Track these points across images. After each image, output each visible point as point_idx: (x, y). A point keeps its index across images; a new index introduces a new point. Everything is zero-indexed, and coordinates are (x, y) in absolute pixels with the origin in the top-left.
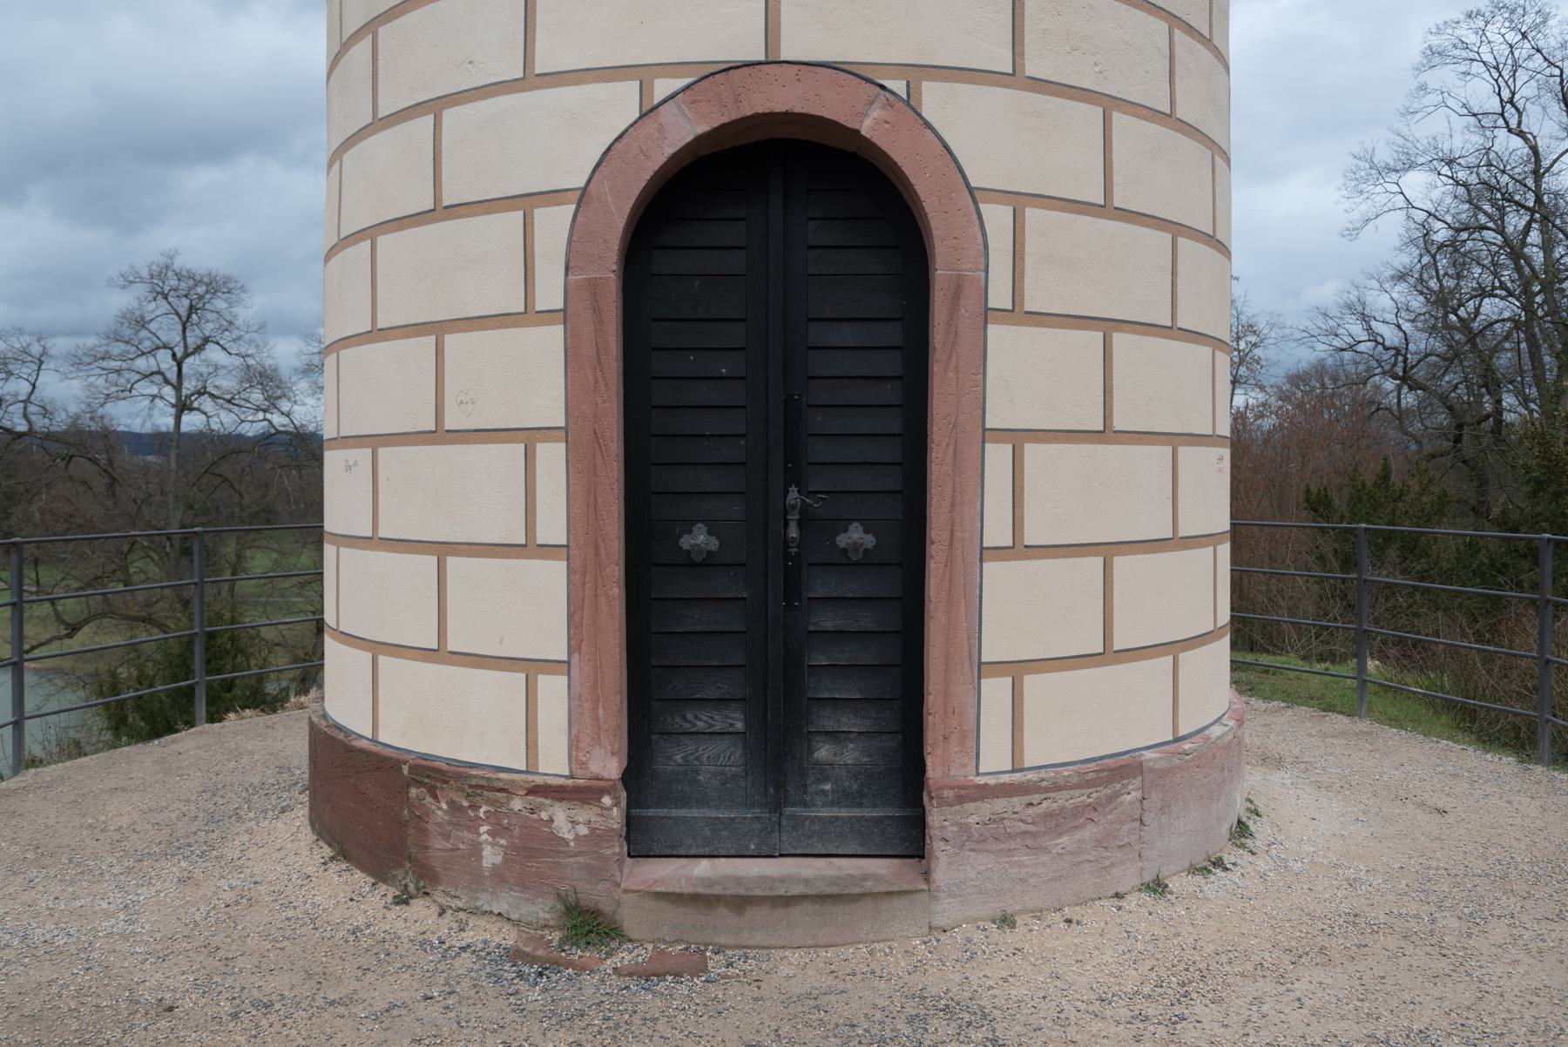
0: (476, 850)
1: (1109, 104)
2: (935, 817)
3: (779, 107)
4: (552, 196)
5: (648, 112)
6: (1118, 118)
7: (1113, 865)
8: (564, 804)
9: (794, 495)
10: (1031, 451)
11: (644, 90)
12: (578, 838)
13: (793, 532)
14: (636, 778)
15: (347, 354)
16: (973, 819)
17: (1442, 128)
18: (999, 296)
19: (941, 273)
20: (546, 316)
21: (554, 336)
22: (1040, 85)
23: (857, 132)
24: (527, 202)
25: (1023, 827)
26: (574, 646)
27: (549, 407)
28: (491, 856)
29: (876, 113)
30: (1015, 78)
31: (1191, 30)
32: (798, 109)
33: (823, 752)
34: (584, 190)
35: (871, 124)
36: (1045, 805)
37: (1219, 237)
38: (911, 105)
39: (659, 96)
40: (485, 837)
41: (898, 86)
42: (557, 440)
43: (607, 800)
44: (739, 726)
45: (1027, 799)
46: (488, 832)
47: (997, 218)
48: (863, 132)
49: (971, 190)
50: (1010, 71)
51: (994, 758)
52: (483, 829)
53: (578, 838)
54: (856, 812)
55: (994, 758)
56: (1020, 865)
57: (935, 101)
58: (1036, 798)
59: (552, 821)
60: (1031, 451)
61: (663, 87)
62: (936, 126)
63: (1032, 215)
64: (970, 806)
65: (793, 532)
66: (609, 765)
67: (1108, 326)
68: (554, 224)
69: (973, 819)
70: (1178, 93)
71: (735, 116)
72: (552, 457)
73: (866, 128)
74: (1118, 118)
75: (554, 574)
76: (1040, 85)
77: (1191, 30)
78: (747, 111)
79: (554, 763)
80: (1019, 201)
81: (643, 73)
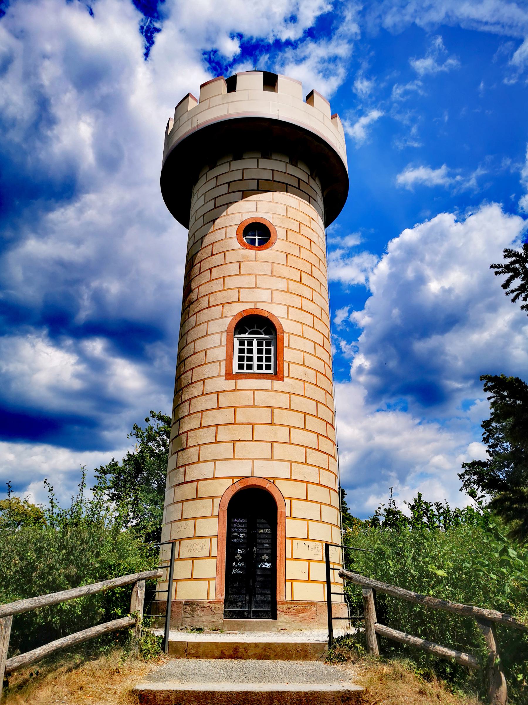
1: (307, 483)
7: (311, 622)
10: (295, 584)
11: (233, 480)
15: (176, 523)
23: (265, 488)
24: (213, 497)
25: (293, 611)
29: (268, 485)
31: (331, 456)
35: (268, 486)
41: (272, 481)
43: (222, 603)
45: (294, 605)
47: (288, 502)
49: (283, 497)
56: (293, 618)
60: (295, 584)
61: (236, 480)
63: (293, 501)
64: (284, 606)
67: (308, 520)
68: (217, 501)
70: (321, 480)
73: (267, 487)
75: (225, 348)
76: (294, 480)
77: (331, 456)
79: (212, 598)
80: (291, 499)
81: (232, 478)
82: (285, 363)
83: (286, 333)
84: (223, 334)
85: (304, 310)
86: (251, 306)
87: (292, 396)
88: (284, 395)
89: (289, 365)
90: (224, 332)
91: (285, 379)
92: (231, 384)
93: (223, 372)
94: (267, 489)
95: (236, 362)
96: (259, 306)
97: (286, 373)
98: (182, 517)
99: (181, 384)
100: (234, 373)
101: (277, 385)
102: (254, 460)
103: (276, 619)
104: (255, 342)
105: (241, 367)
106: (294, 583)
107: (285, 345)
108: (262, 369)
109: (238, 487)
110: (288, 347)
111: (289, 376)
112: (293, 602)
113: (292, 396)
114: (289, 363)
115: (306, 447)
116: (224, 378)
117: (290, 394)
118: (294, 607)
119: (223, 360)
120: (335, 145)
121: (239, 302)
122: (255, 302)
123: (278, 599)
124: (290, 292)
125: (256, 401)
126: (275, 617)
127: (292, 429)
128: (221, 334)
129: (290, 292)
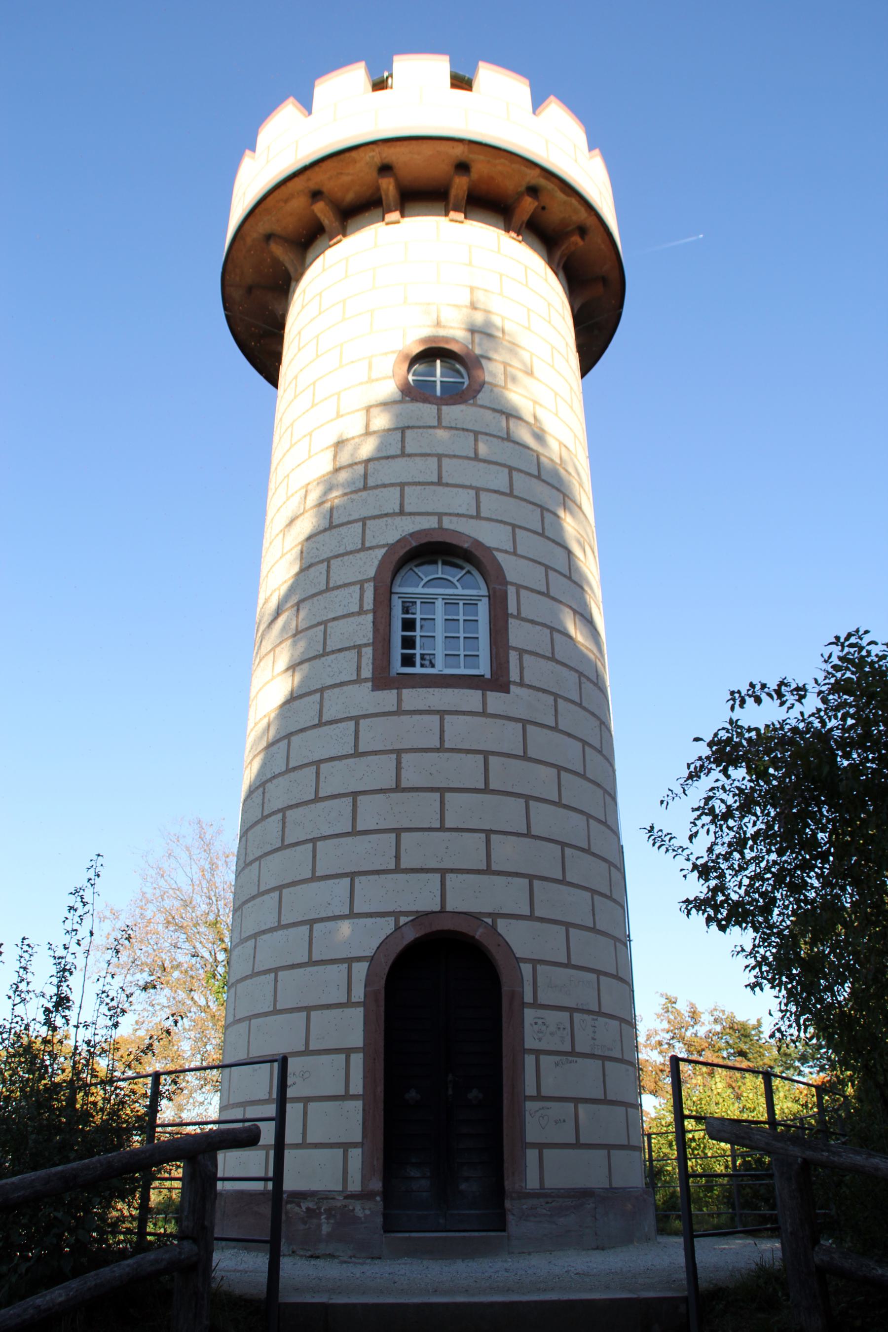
0: (319, 1226)
1: (568, 925)
2: (508, 1204)
3: (446, 928)
4: (359, 959)
5: (398, 928)
6: (571, 930)
8: (360, 1202)
9: (450, 1077)
11: (397, 921)
12: (366, 1216)
13: (450, 1092)
14: (387, 1194)
16: (525, 1207)
17: (87, 1016)
18: (528, 998)
19: (505, 989)
20: (356, 1004)
21: (359, 1012)
22: (542, 920)
23: (473, 937)
24: (350, 961)
26: (364, 1135)
27: (357, 1039)
28: (325, 1229)
30: (531, 917)
32: (452, 929)
33: (463, 1186)
34: (373, 957)
35: (479, 934)
36: (553, 1204)
37: (620, 975)
38: (494, 927)
39: (401, 923)
40: (324, 1220)
41: (489, 921)
42: (360, 1052)
44: (428, 1174)
46: (325, 1218)
47: (526, 969)
48: (477, 937)
50: (529, 914)
51: (532, 1183)
52: (323, 1217)
53: (366, 1216)
54: (477, 1212)
55: (532, 1183)
57: (502, 926)
58: (550, 1200)
59: (354, 1209)
61: (403, 920)
62: (503, 935)
65: (450, 1092)
66: (377, 1185)
68: (361, 970)
69: (525, 1207)
71: (428, 930)
72: (357, 1060)
74: (571, 930)
75: (370, 617)
76: (542, 920)
78: (434, 929)
79: (355, 1186)
80: (535, 962)
81: (397, 914)
82: (511, 651)
83: (512, 584)
84: (366, 585)
85: (548, 538)
86: (430, 523)
87: (529, 728)
88: (512, 724)
89: (521, 660)
90: (367, 580)
91: (513, 688)
92: (387, 699)
93: (367, 672)
94: (477, 941)
95: (397, 651)
96: (447, 523)
97: (514, 675)
98: (311, 931)
99: (522, 962)
100: (393, 673)
101: (496, 701)
102: (445, 874)
103: (504, 1230)
104: (439, 604)
105: (408, 661)
106: (545, 1151)
107: (510, 611)
108: (460, 667)
109: (410, 935)
110: (518, 617)
111: (521, 684)
112: (542, 1194)
113: (529, 728)
114: (522, 652)
115: (563, 845)
116: (370, 684)
117: (525, 723)
118: (547, 1203)
119: (366, 645)
120: (600, 206)
121: (404, 456)
122: (440, 515)
123: (507, 1184)
124: (517, 497)
125: (446, 738)
126: (502, 1227)
127: (531, 803)
128: (362, 590)
129: (517, 497)
